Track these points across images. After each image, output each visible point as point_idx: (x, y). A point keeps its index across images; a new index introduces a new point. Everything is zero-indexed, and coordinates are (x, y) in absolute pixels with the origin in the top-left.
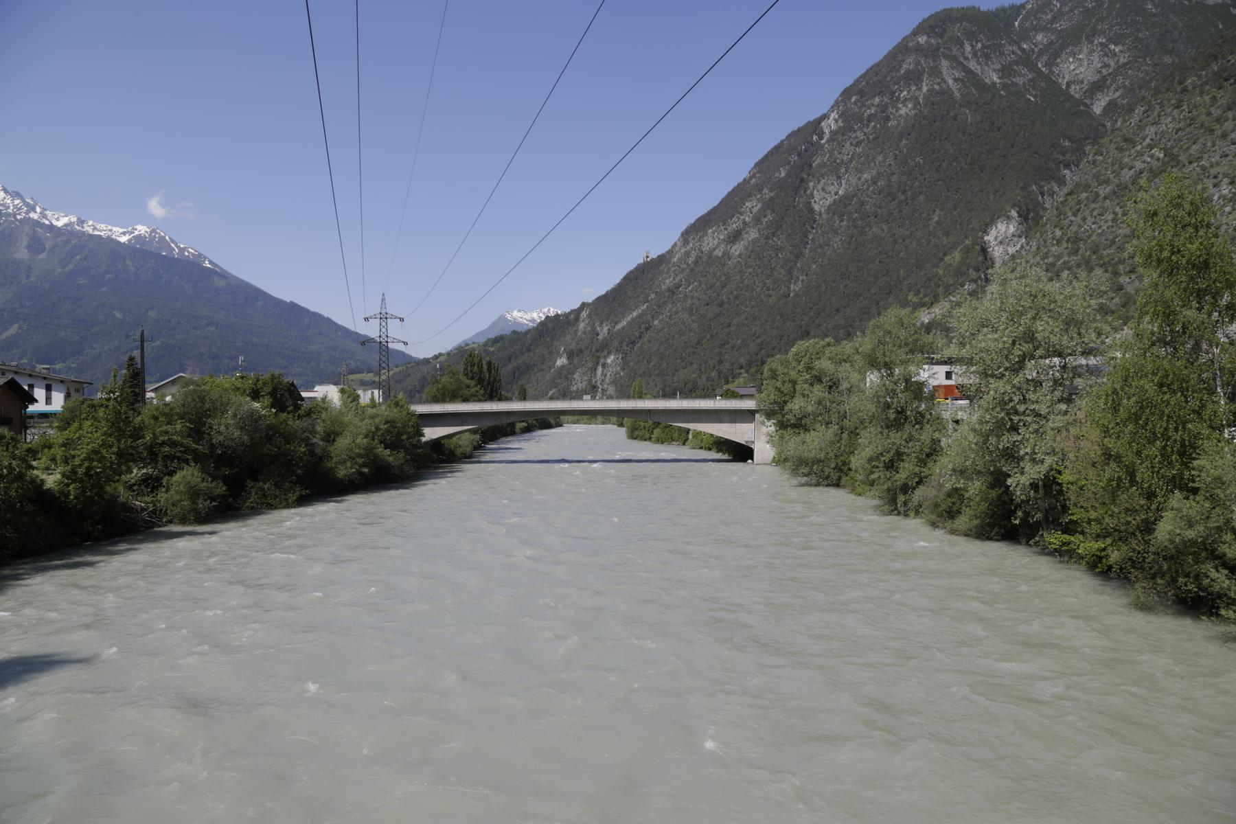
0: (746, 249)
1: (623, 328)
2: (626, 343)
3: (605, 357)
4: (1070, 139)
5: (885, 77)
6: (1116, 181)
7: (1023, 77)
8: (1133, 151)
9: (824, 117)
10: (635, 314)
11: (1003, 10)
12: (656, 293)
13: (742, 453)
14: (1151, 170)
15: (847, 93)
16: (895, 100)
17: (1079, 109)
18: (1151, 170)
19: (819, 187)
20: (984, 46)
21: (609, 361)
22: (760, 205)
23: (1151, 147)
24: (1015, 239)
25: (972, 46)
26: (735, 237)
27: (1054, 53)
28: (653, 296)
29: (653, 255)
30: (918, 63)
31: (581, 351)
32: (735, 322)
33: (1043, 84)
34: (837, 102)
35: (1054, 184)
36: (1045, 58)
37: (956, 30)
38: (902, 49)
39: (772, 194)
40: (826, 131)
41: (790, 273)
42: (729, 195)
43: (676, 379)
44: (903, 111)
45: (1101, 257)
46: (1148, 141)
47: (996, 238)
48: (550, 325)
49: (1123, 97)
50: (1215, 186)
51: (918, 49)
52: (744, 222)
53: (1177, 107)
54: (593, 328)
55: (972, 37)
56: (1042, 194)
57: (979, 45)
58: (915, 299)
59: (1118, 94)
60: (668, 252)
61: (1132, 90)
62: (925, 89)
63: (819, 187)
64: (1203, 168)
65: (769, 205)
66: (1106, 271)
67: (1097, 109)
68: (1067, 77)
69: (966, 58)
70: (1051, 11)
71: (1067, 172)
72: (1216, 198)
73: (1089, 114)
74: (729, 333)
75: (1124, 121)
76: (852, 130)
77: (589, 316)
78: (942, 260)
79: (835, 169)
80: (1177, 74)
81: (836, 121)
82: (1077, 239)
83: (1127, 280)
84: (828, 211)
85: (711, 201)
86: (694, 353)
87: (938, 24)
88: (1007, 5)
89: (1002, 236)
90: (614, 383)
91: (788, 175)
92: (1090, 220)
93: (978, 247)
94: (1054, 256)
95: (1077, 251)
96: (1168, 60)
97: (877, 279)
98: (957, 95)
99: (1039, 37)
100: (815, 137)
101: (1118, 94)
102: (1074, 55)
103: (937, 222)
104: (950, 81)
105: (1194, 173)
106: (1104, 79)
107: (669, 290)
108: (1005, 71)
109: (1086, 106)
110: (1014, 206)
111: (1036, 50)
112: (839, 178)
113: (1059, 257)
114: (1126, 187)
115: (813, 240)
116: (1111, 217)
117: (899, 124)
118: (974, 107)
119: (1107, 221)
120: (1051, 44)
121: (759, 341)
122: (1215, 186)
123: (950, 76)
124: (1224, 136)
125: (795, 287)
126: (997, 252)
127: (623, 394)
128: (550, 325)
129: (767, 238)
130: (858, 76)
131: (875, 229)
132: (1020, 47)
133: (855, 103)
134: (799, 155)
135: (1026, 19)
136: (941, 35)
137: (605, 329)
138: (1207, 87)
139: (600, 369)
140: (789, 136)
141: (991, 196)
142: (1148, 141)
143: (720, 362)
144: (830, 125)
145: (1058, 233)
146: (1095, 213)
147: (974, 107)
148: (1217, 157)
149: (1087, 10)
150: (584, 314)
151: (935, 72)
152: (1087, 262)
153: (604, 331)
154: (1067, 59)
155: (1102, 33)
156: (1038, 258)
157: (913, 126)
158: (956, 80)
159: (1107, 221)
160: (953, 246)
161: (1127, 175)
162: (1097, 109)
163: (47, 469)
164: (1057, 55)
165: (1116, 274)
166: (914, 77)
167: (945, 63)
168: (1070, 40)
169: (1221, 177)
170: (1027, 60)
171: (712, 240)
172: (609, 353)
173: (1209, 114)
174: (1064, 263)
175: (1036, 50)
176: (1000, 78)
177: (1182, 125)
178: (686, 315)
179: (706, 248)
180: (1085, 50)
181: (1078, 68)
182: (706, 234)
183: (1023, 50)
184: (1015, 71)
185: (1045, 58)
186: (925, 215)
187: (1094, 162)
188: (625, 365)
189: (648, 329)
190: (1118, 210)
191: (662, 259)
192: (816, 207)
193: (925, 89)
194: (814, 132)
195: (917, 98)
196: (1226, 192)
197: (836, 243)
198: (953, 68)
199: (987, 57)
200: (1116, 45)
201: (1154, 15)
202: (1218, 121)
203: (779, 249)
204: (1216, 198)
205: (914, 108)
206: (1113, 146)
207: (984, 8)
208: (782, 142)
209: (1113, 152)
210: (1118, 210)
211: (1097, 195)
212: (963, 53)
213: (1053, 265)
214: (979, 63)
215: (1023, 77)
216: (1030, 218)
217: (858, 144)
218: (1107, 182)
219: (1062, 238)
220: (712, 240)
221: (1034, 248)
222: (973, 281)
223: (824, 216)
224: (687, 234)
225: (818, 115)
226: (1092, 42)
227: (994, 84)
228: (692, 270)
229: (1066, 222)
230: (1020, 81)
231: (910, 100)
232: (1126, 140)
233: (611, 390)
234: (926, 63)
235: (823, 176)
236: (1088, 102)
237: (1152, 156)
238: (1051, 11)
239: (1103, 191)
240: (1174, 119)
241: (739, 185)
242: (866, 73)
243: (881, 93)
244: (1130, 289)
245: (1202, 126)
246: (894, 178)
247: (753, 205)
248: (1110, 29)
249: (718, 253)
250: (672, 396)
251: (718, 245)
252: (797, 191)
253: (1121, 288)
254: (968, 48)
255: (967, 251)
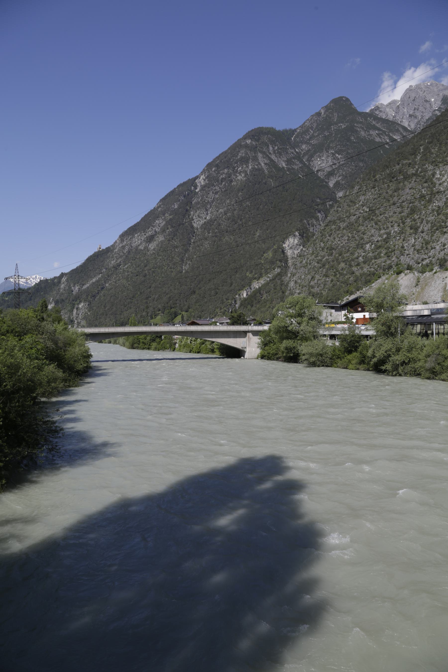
0: (157, 245)
1: (88, 288)
2: (90, 296)
3: (78, 304)
4: (320, 199)
5: (230, 159)
6: (348, 221)
7: (297, 166)
8: (355, 207)
9: (197, 177)
10: (94, 280)
11: (286, 131)
12: (106, 269)
13: (236, 353)
14: (364, 217)
15: (209, 166)
16: (235, 172)
17: (323, 184)
18: (364, 217)
19: (196, 214)
20: (278, 148)
21: (80, 306)
22: (164, 222)
23: (363, 206)
24: (298, 247)
25: (273, 148)
26: (151, 239)
27: (311, 155)
28: (104, 270)
29: (104, 247)
30: (247, 154)
31: (63, 300)
32: (153, 285)
33: (306, 170)
34: (204, 170)
35: (314, 220)
36: (306, 157)
37: (265, 138)
38: (237, 146)
39: (171, 217)
40: (198, 184)
41: (182, 260)
42: (146, 216)
43: (122, 316)
44: (239, 178)
45: (343, 258)
46: (361, 203)
47: (289, 246)
48: (43, 285)
49: (342, 180)
50: (392, 226)
51: (246, 146)
52: (155, 231)
53: (374, 188)
54: (70, 287)
55: (273, 143)
56: (309, 225)
57: (276, 148)
58: (250, 276)
59: (340, 178)
60: (112, 246)
61: (346, 177)
62: (250, 167)
63: (196, 214)
64: (386, 217)
65: (169, 223)
66: (346, 264)
67: (331, 184)
68: (317, 168)
69: (270, 154)
70: (309, 134)
71: (319, 214)
72: (392, 232)
73: (327, 187)
74: (150, 292)
75: (350, 192)
76: (213, 185)
77: (67, 281)
78: (263, 256)
79: (204, 205)
80: (372, 172)
81: (205, 180)
82: (331, 249)
83: (356, 269)
84: (201, 227)
85: (137, 219)
86: (131, 302)
87: (257, 134)
88: (288, 129)
89: (291, 245)
90: (84, 318)
91: (179, 207)
92: (337, 239)
93: (281, 250)
94: (321, 256)
95: (332, 254)
96: (361, 164)
97: (229, 264)
98: (266, 171)
99: (304, 147)
100: (192, 188)
101: (340, 178)
102: (320, 157)
103: (259, 236)
104: (263, 164)
105: (383, 220)
106: (334, 170)
107: (114, 267)
108: (289, 162)
109: (326, 182)
110: (297, 230)
111: (302, 153)
112: (207, 210)
113: (324, 257)
114: (353, 224)
115: (194, 242)
116: (347, 238)
117: (237, 184)
118: (274, 178)
119: (345, 240)
120: (309, 150)
121: (169, 296)
122: (392, 226)
123: (262, 162)
124: (394, 204)
125: (186, 268)
126: (289, 253)
127: (90, 325)
128: (43, 285)
129: (169, 240)
130: (215, 157)
131: (227, 238)
132: (295, 151)
133: (214, 171)
134: (184, 196)
135: (297, 136)
136: (257, 140)
137: (77, 288)
138: (385, 180)
139: (75, 311)
140: (178, 186)
141: (285, 224)
142: (361, 203)
143: (147, 307)
144: (201, 181)
145: (322, 245)
146: (339, 236)
147: (274, 178)
148: (392, 213)
149: (325, 136)
150: (64, 279)
151: (255, 159)
152: (337, 260)
153: (76, 289)
154: (317, 159)
155: (332, 148)
156: (313, 257)
157: (245, 186)
158: (265, 164)
159: (345, 240)
160: (268, 249)
161: (353, 218)
162: (331, 184)
163: (444, 361)
164: (312, 156)
165: (351, 266)
166: (244, 160)
167: (260, 155)
168: (318, 149)
169: (394, 222)
170: (298, 157)
171: (138, 240)
172: (80, 302)
173: (387, 193)
174: (326, 260)
175: (302, 153)
176: (286, 165)
177: (376, 196)
178: (124, 281)
179: (134, 245)
180: (325, 156)
181: (322, 163)
182: (134, 236)
183: (297, 152)
184: (293, 162)
185: (306, 157)
186: (252, 232)
187: (337, 211)
188: (90, 307)
189: (103, 288)
190: (350, 235)
191: (108, 250)
192: (195, 225)
193: (250, 167)
194: (192, 185)
195: (246, 172)
196: (396, 230)
197: (207, 244)
198: (264, 158)
199: (280, 154)
200: (339, 154)
201: (354, 143)
202: (391, 196)
203: (177, 247)
204: (392, 232)
205: (245, 176)
206: (345, 204)
207: (277, 129)
208: (175, 189)
209: (346, 207)
210: (350, 235)
211: (340, 227)
212: (269, 151)
213: (321, 260)
214: (276, 157)
215: (297, 166)
216: (306, 237)
217: (216, 193)
218: (344, 221)
219: (324, 247)
220: (138, 240)
221: (311, 252)
222: (279, 267)
223: (199, 230)
224: (123, 236)
225: (194, 176)
226: (328, 152)
227: (283, 168)
228: (127, 256)
229: (326, 240)
230: (296, 167)
231: (243, 172)
232: (351, 202)
233: (83, 323)
234: (251, 154)
235: (198, 208)
236: (327, 181)
237: (363, 210)
238: (309, 134)
239: (342, 225)
240: (372, 193)
241: (151, 211)
242: (219, 156)
243: (228, 167)
244: (357, 273)
245: (384, 198)
246: (235, 212)
247: (160, 223)
248: (336, 146)
249: (141, 247)
250: (123, 324)
251: (141, 243)
252: (184, 216)
253: (353, 273)
254: (271, 148)
255: (275, 251)
